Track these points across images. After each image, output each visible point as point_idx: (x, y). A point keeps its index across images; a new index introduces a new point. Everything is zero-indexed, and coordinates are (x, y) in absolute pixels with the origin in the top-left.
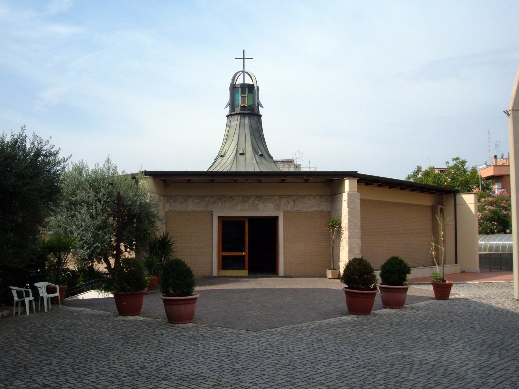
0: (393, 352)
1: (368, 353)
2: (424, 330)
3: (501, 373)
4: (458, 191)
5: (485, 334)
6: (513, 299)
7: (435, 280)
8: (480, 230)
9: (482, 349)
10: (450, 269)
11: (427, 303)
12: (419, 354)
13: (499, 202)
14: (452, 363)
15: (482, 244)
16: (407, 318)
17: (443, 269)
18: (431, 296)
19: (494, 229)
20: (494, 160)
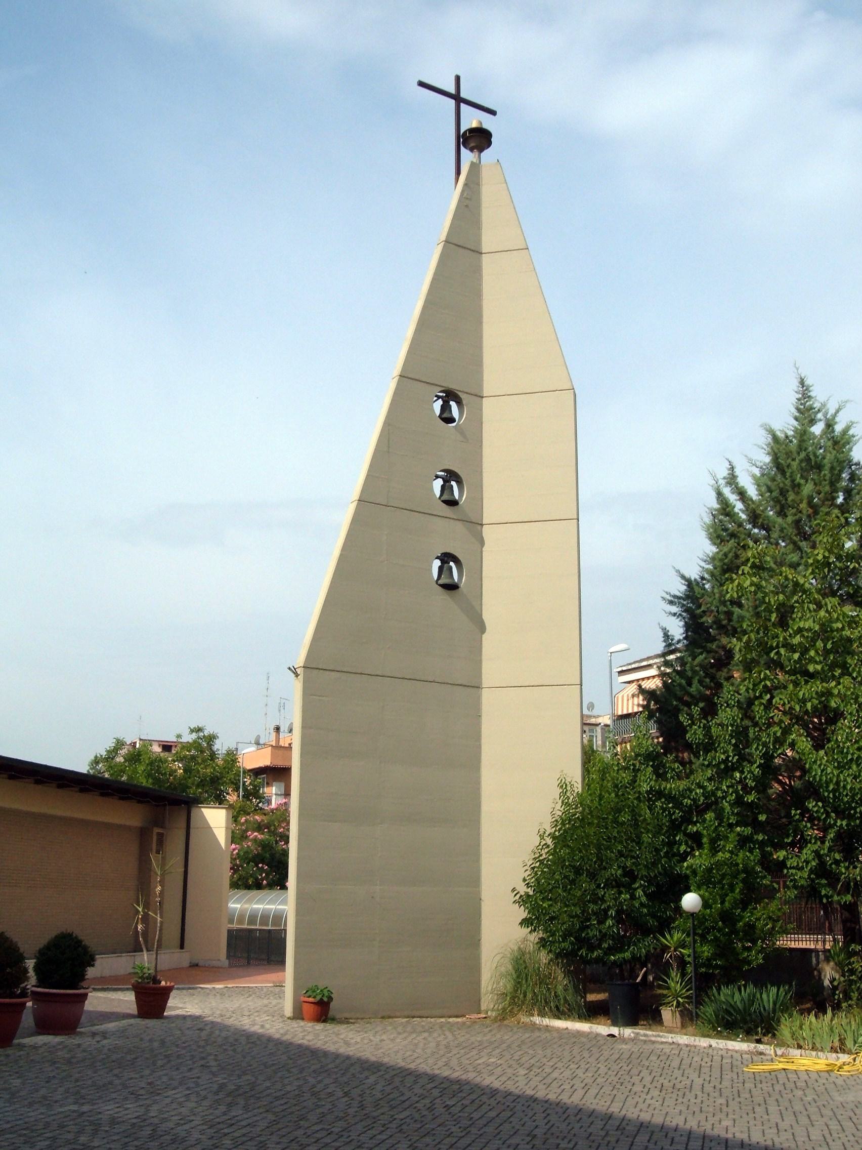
0: (61, 1106)
1: (14, 1110)
2: (116, 1072)
3: (244, 1131)
4: (197, 801)
5: (225, 1076)
6: (283, 1016)
7: (140, 981)
8: (234, 880)
9: (217, 1097)
10: (170, 958)
11: (121, 1025)
12: (108, 1109)
13: (274, 825)
14: (165, 1120)
15: (236, 908)
16: (84, 1051)
17: (156, 959)
18: (129, 1011)
19: (263, 879)
20: (274, 734)
